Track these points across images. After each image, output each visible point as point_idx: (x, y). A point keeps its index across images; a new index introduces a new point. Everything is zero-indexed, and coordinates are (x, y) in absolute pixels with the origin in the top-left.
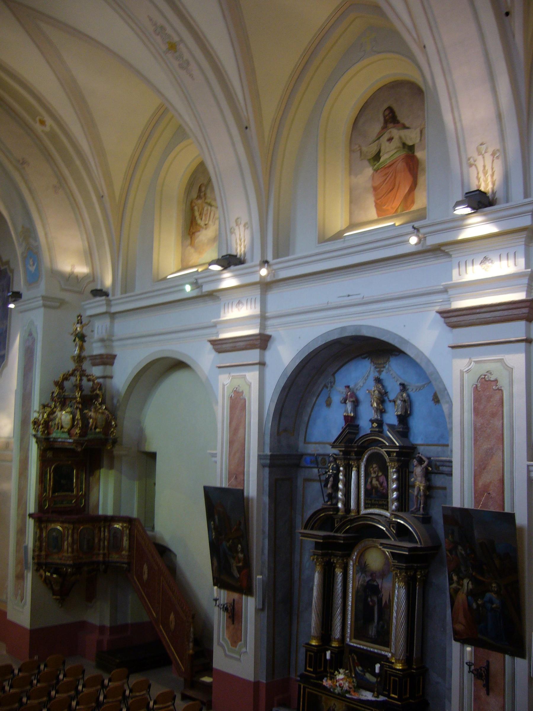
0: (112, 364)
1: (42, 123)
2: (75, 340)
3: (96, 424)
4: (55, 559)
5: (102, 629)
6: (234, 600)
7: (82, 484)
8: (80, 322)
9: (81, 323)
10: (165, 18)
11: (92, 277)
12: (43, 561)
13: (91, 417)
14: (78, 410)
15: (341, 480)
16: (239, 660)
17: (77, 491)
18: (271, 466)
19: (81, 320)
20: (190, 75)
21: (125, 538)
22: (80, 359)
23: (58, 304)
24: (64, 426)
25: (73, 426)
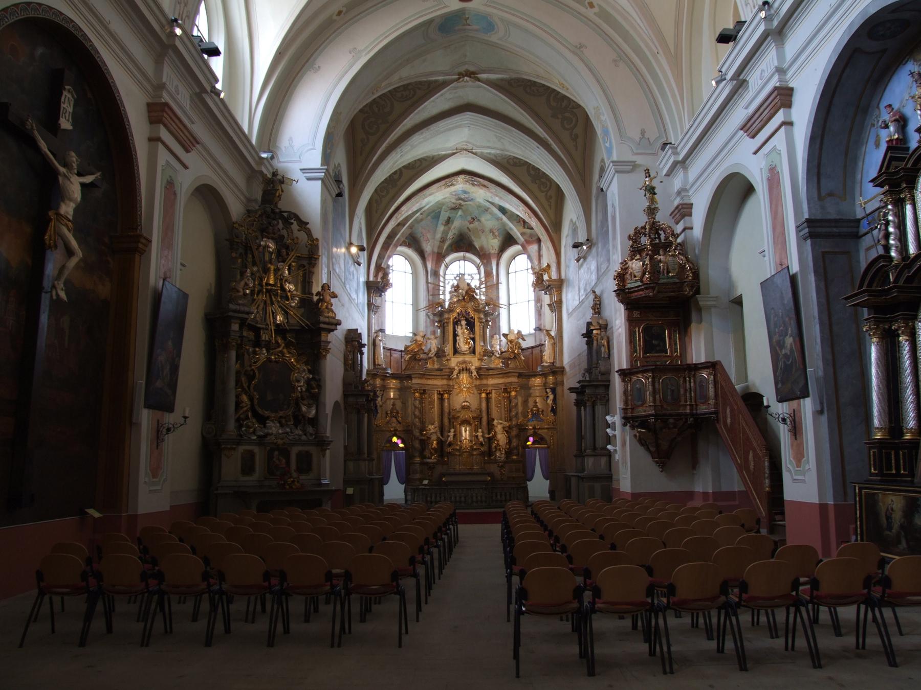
2: (645, 195)
3: (668, 268)
4: (641, 412)
5: (705, 495)
6: (794, 410)
7: (676, 344)
9: (650, 176)
12: (629, 415)
13: (660, 261)
14: (648, 257)
15: (892, 221)
16: (803, 481)
17: (671, 352)
18: (812, 236)
21: (711, 386)
23: (631, 167)
24: (636, 274)
25: (644, 274)
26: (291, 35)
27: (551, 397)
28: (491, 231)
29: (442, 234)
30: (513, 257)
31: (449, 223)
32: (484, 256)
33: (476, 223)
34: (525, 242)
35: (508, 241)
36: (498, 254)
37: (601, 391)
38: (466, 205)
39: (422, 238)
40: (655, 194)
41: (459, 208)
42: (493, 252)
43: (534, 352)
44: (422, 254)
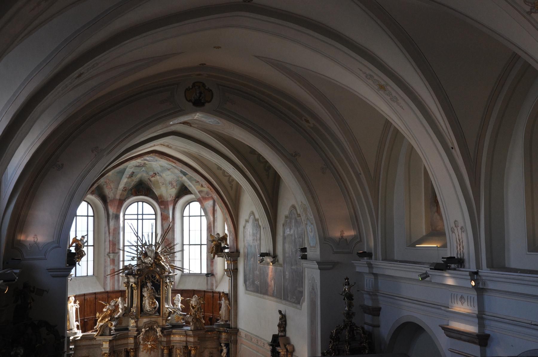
0: (379, 315)
1: (307, 121)
2: (344, 299)
8: (348, 284)
9: (349, 284)
10: (371, 70)
11: (359, 239)
19: (348, 282)
20: (400, 106)
22: (349, 315)
23: (331, 266)
26: (69, 237)
27: (225, 351)
28: (171, 183)
29: (125, 185)
30: (188, 203)
31: (132, 177)
32: (161, 202)
33: (158, 177)
34: (202, 199)
35: (183, 191)
36: (175, 200)
37: (236, 262)
38: (149, 164)
39: (105, 186)
40: (353, 299)
41: (143, 166)
42: (169, 199)
43: (206, 295)
44: (104, 199)
